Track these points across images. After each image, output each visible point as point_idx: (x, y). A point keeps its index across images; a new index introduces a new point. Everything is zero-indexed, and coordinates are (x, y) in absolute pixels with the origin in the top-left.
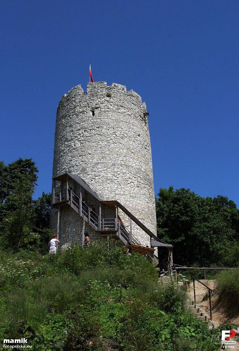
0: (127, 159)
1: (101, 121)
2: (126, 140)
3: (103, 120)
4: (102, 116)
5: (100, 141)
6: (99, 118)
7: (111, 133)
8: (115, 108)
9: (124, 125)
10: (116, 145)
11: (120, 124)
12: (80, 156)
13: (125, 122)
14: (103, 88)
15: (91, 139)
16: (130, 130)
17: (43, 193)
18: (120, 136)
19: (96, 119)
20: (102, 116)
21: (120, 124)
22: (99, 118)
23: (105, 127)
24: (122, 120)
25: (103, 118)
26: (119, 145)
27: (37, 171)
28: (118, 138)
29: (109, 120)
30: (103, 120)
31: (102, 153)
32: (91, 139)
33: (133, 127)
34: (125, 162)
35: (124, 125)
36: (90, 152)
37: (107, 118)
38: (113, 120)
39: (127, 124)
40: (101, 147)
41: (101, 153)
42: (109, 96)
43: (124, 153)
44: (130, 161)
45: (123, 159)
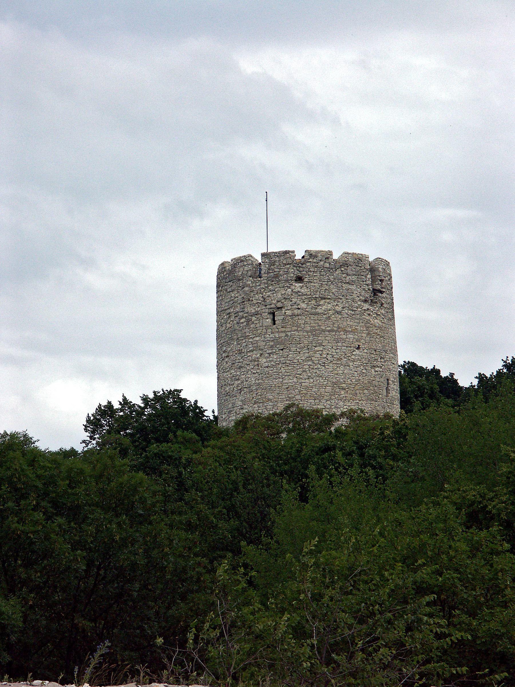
0: (333, 404)
1: (287, 335)
2: (330, 367)
3: (289, 334)
4: (289, 326)
5: (286, 376)
6: (283, 329)
7: (303, 358)
8: (311, 307)
9: (327, 338)
10: (312, 380)
11: (320, 338)
12: (255, 403)
13: (329, 331)
14: (288, 266)
15: (270, 372)
16: (340, 344)
17: (206, 410)
18: (320, 363)
19: (278, 332)
20: (289, 326)
21: (320, 338)
22: (283, 329)
23: (293, 349)
24: (324, 328)
25: (289, 329)
26: (318, 381)
27: (180, 391)
28: (316, 367)
29: (301, 333)
30: (289, 334)
31: (290, 398)
32: (270, 372)
33: (344, 337)
34: (328, 410)
35: (327, 338)
36: (271, 397)
37: (297, 330)
38: (307, 332)
39: (334, 333)
40: (287, 388)
41: (288, 399)
42: (299, 279)
43: (326, 394)
44: (338, 408)
45: (325, 406)
